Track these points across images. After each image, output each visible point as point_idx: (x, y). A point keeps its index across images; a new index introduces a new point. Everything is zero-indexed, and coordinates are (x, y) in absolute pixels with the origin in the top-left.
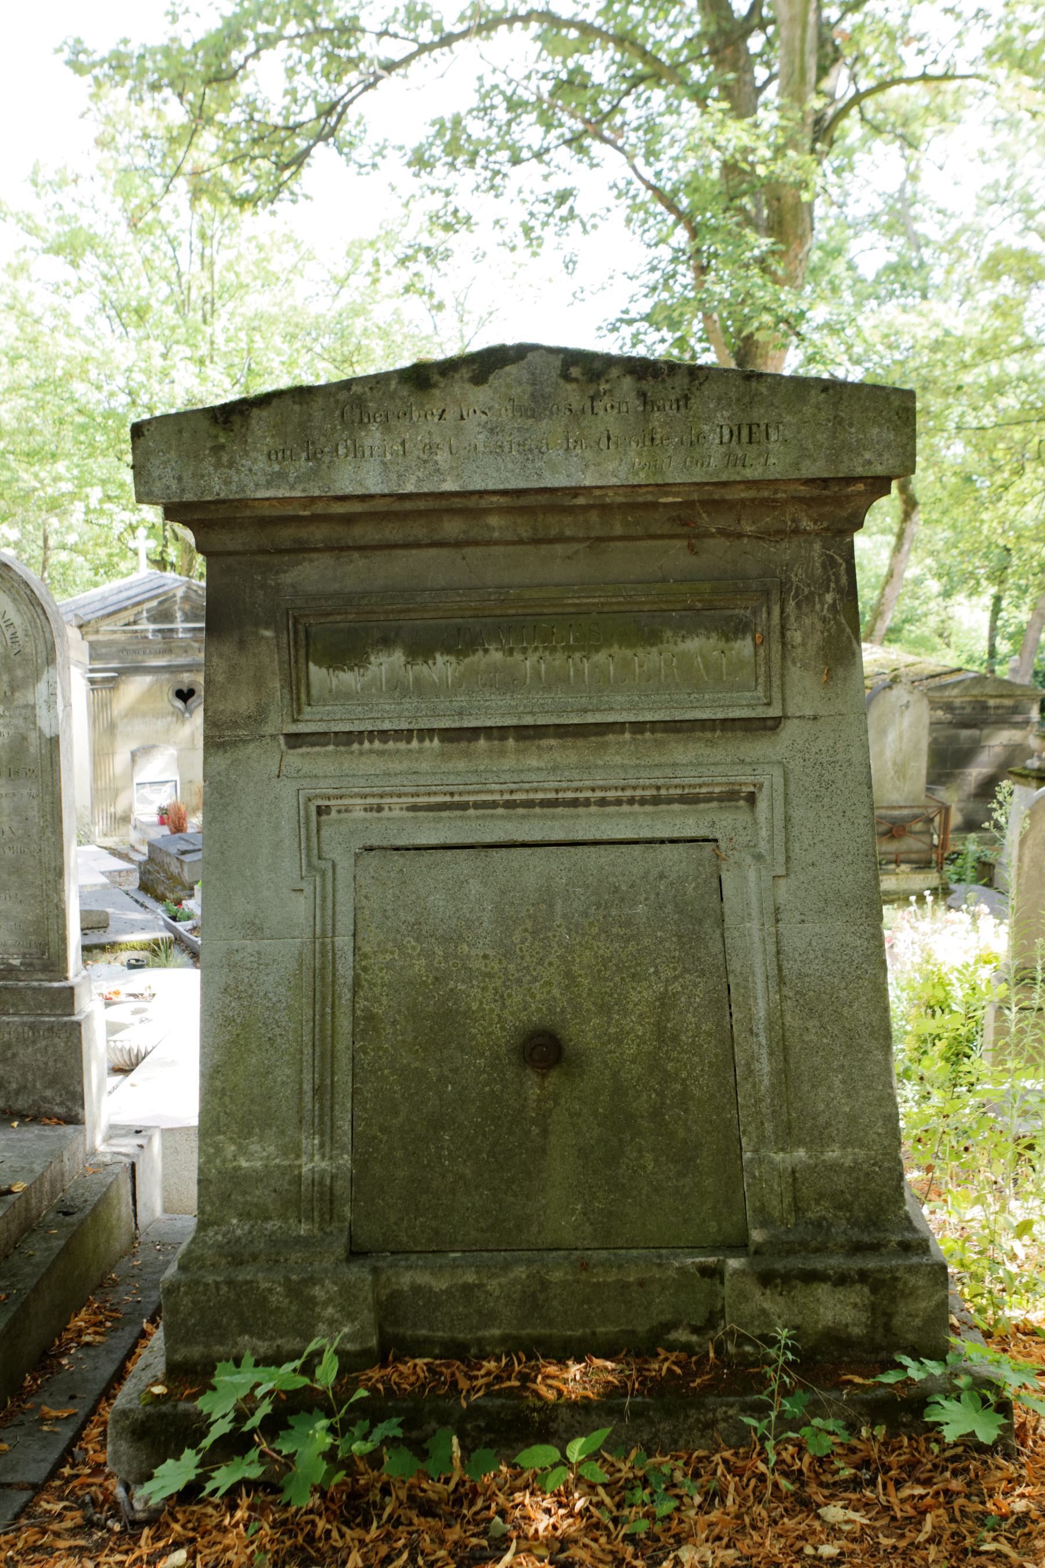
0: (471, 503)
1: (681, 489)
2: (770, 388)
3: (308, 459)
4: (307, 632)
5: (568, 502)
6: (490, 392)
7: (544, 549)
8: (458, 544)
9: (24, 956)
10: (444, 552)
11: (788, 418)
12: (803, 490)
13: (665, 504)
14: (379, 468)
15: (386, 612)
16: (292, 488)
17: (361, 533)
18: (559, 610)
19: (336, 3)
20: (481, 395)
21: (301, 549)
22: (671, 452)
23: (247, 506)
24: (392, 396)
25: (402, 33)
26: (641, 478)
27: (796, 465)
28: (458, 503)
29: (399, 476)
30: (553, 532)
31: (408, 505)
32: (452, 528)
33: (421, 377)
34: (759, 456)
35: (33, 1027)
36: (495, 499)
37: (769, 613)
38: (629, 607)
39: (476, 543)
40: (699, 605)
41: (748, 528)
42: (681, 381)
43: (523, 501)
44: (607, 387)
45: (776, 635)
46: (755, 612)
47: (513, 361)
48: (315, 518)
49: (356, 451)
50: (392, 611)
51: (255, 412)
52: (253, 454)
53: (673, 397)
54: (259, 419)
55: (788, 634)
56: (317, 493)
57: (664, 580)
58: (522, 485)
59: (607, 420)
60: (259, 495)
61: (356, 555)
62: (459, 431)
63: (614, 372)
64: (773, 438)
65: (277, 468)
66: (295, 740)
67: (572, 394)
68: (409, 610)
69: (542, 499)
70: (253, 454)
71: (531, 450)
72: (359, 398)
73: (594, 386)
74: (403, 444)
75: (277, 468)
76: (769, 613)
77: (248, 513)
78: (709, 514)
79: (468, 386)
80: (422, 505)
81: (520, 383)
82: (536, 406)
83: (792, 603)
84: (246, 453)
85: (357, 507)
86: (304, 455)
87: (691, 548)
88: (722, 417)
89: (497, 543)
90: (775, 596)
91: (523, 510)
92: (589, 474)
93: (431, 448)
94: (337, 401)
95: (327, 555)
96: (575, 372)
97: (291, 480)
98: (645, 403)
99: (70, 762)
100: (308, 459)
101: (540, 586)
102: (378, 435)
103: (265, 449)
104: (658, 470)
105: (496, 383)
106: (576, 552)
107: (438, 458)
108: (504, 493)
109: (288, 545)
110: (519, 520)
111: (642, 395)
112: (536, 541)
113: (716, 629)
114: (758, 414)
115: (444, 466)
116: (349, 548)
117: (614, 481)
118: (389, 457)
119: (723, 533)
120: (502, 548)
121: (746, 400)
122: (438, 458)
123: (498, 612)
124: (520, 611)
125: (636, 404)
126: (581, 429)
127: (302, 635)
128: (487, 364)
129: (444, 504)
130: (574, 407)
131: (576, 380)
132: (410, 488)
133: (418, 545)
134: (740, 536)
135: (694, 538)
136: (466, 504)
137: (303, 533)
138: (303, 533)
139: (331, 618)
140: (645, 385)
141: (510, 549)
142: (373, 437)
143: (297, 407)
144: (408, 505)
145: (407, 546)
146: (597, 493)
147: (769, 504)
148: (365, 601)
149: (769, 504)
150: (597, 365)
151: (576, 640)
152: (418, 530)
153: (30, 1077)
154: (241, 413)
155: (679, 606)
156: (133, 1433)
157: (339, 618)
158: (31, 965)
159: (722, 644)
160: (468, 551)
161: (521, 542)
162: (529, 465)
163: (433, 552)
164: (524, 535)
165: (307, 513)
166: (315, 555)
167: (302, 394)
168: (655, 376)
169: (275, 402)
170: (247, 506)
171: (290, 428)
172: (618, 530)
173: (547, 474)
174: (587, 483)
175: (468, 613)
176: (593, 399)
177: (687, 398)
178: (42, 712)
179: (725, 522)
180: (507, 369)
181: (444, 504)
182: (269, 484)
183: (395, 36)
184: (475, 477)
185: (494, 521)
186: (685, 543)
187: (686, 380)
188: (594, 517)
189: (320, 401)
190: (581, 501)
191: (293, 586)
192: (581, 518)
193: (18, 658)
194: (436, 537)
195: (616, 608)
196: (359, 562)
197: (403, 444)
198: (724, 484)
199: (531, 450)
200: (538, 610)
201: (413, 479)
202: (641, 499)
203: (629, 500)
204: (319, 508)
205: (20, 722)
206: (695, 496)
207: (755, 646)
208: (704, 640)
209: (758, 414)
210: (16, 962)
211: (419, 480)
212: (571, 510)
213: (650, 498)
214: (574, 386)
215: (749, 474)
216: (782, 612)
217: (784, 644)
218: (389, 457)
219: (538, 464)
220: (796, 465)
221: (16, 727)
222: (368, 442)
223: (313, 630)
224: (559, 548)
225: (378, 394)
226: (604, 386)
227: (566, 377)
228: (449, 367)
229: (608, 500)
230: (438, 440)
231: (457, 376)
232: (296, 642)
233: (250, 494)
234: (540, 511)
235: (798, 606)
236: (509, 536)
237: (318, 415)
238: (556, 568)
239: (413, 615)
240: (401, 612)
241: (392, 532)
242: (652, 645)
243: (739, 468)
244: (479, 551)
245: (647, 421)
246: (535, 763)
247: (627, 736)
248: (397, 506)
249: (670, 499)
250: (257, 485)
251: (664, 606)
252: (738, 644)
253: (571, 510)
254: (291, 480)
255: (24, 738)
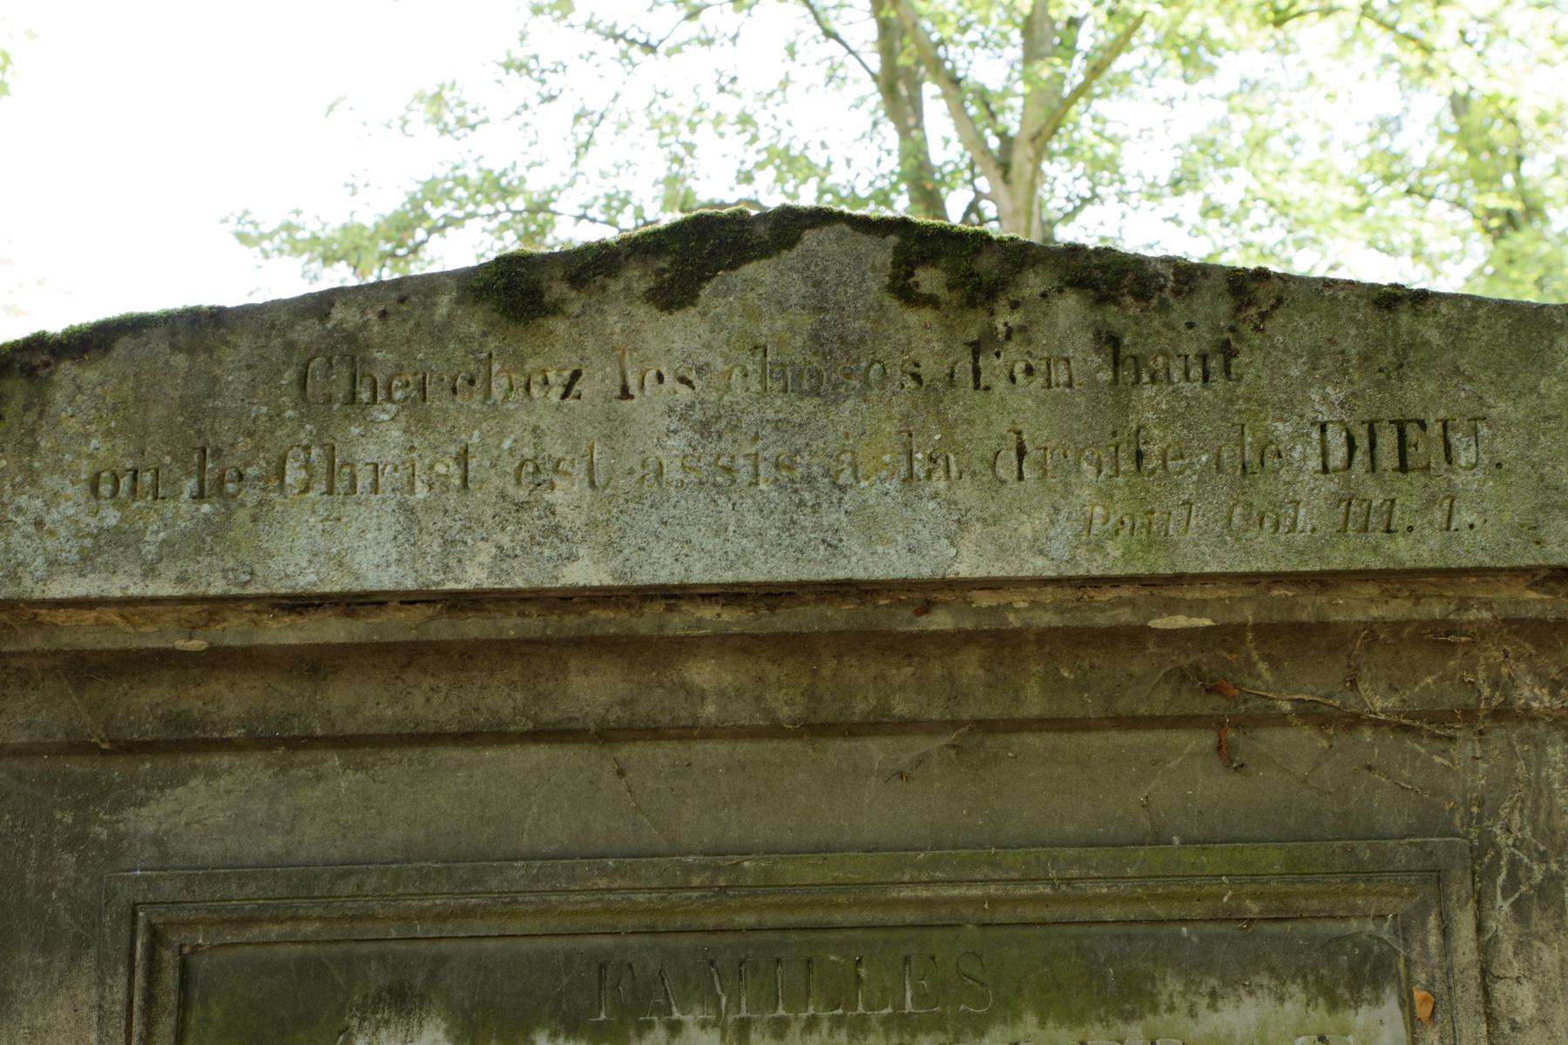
0: (645, 621)
1: (1210, 593)
2: (1445, 328)
3: (200, 496)
4: (184, 968)
5: (905, 622)
6: (703, 329)
7: (837, 750)
8: (606, 735)
10: (567, 756)
11: (1500, 408)
12: (1535, 602)
13: (1166, 636)
14: (391, 521)
15: (403, 918)
16: (150, 571)
17: (353, 700)
18: (877, 916)
20: (677, 336)
21: (186, 743)
22: (1190, 490)
23: (35, 622)
24: (439, 334)
25: (602, 218)
26: (1111, 559)
27: (1532, 531)
28: (607, 620)
29: (448, 543)
30: (861, 707)
31: (474, 627)
32: (592, 690)
33: (518, 290)
34: (1431, 502)
36: (708, 613)
37: (1445, 933)
38: (1065, 911)
39: (654, 733)
40: (1254, 908)
41: (1379, 703)
42: (1214, 308)
43: (782, 621)
44: (1015, 319)
45: (1469, 995)
46: (1403, 930)
47: (766, 251)
48: (219, 660)
49: (335, 476)
50: (421, 915)
51: (67, 370)
52: (50, 482)
53: (1191, 349)
55: (1499, 989)
56: (218, 587)
57: (1159, 839)
58: (785, 571)
59: (1016, 404)
60: (56, 590)
61: (334, 760)
62: (615, 428)
63: (1033, 283)
64: (1464, 457)
65: (111, 517)
67: (921, 336)
68: (467, 913)
69: (838, 615)
70: (50, 482)
71: (809, 480)
72: (351, 338)
73: (981, 316)
74: (463, 458)
75: (111, 517)
76: (1445, 933)
77: (36, 642)
78: (1274, 663)
79: (642, 311)
80: (511, 626)
81: (782, 306)
82: (826, 366)
83: (1504, 906)
84: (32, 477)
85: (333, 630)
86: (190, 485)
87: (1223, 750)
88: (1323, 401)
89: (709, 732)
90: (1459, 886)
91: (794, 646)
92: (967, 546)
93: (538, 472)
94: (290, 346)
95: (255, 759)
96: (929, 279)
97: (149, 550)
98: (1116, 363)
100: (200, 496)
101: (823, 849)
102: (395, 433)
103: (86, 469)
104: (1157, 540)
105: (719, 307)
106: (920, 761)
107: (556, 497)
108: (733, 595)
109: (149, 730)
110: (773, 673)
111: (1110, 342)
112: (815, 729)
113: (1301, 973)
114: (1417, 394)
115: (569, 517)
116: (310, 742)
117: (1036, 566)
118: (421, 492)
119: (1313, 715)
120: (723, 748)
121: (1387, 358)
122: (556, 497)
123: (711, 921)
124: (770, 918)
125: (1090, 362)
126: (948, 427)
127: (170, 978)
128: (697, 253)
129: (571, 623)
130: (928, 368)
131: (932, 301)
132: (474, 576)
133: (499, 736)
134: (1355, 721)
135: (1232, 725)
136: (626, 625)
137: (193, 700)
138: (193, 700)
139: (254, 932)
140: (1113, 317)
141: (744, 748)
142: (381, 439)
143: (180, 360)
144: (474, 627)
145: (468, 737)
146: (984, 600)
147: (1438, 638)
148: (348, 886)
149: (1438, 638)
150: (986, 264)
151: (919, 999)
152: (500, 696)
154: (30, 372)
155: (1198, 910)
157: (274, 931)
159: (1319, 1016)
160: (631, 753)
161: (775, 730)
162: (807, 520)
163: (539, 754)
164: (785, 712)
165: (197, 644)
166: (224, 760)
167: (201, 328)
168: (1142, 295)
169: (122, 346)
170: (35, 622)
171: (158, 412)
172: (1034, 703)
173: (852, 544)
174: (964, 570)
175: (630, 922)
176: (976, 349)
177: (1228, 351)
179: (1314, 682)
180: (748, 269)
181: (571, 623)
182: (85, 562)
183: (593, 220)
184: (658, 551)
185: (703, 673)
186: (1208, 739)
187: (1225, 307)
188: (970, 665)
189: (246, 343)
190: (941, 621)
191: (157, 841)
192: (937, 670)
194: (549, 716)
195: (1030, 913)
196: (341, 779)
197: (463, 458)
198: (1324, 581)
199: (809, 480)
200: (819, 916)
201: (486, 553)
202: (1102, 620)
203: (1069, 620)
204: (232, 631)
206: (1248, 614)
207: (1413, 1022)
208: (1269, 1003)
209: (1417, 394)
211: (502, 554)
212: (909, 646)
213: (1125, 616)
214: (927, 315)
215: (1405, 552)
216: (1480, 929)
217: (1491, 1019)
218: (421, 492)
219: (830, 517)
220: (1532, 531)
222: (367, 452)
223: (203, 963)
224: (875, 749)
225: (400, 330)
226: (1005, 319)
227: (904, 291)
228: (592, 266)
229: (1013, 621)
230: (558, 450)
231: (615, 286)
232: (150, 998)
233: (31, 588)
234: (831, 644)
235: (1520, 911)
236: (744, 713)
237: (235, 381)
238: (868, 803)
239: (479, 926)
240: (442, 917)
241: (428, 699)
242: (1129, 1017)
243: (1377, 535)
244: (662, 753)
245: (1124, 409)
248: (443, 629)
249: (1181, 621)
250: (53, 563)
251: (1160, 911)
252: (1363, 1017)
253: (909, 646)
254: (149, 550)
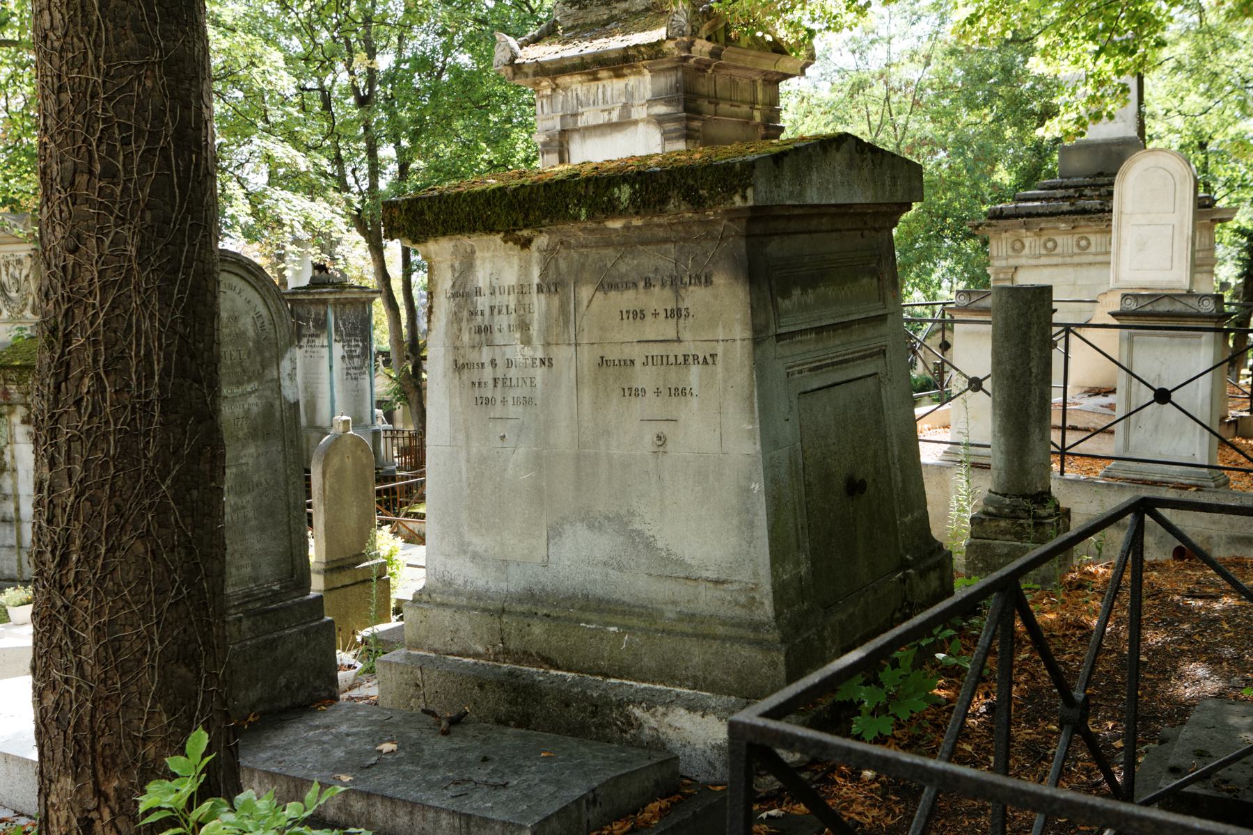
9: (280, 580)
19: (1249, 21)
35: (306, 633)
54: (839, 157)
66: (779, 337)
99: (1164, 285)
153: (306, 674)
156: (751, 746)
158: (287, 587)
160: (815, 235)
178: (286, 383)
193: (266, 343)
205: (268, 393)
210: (276, 588)
221: (267, 398)
246: (837, 342)
247: (813, 335)
255: (272, 406)
